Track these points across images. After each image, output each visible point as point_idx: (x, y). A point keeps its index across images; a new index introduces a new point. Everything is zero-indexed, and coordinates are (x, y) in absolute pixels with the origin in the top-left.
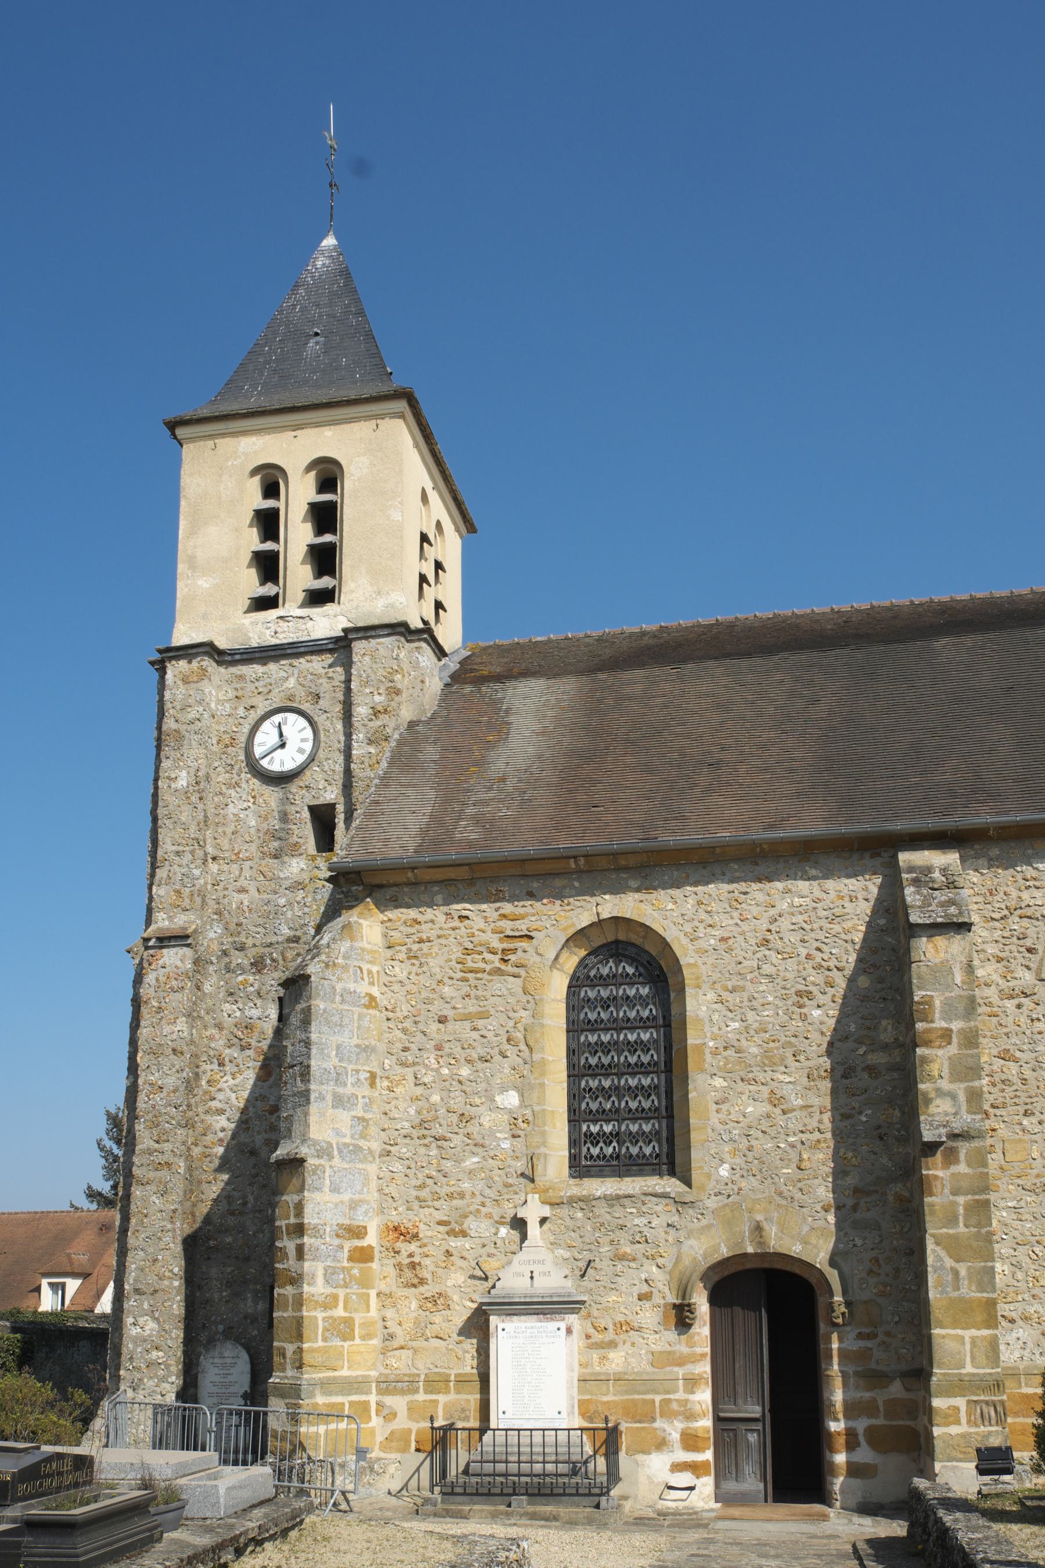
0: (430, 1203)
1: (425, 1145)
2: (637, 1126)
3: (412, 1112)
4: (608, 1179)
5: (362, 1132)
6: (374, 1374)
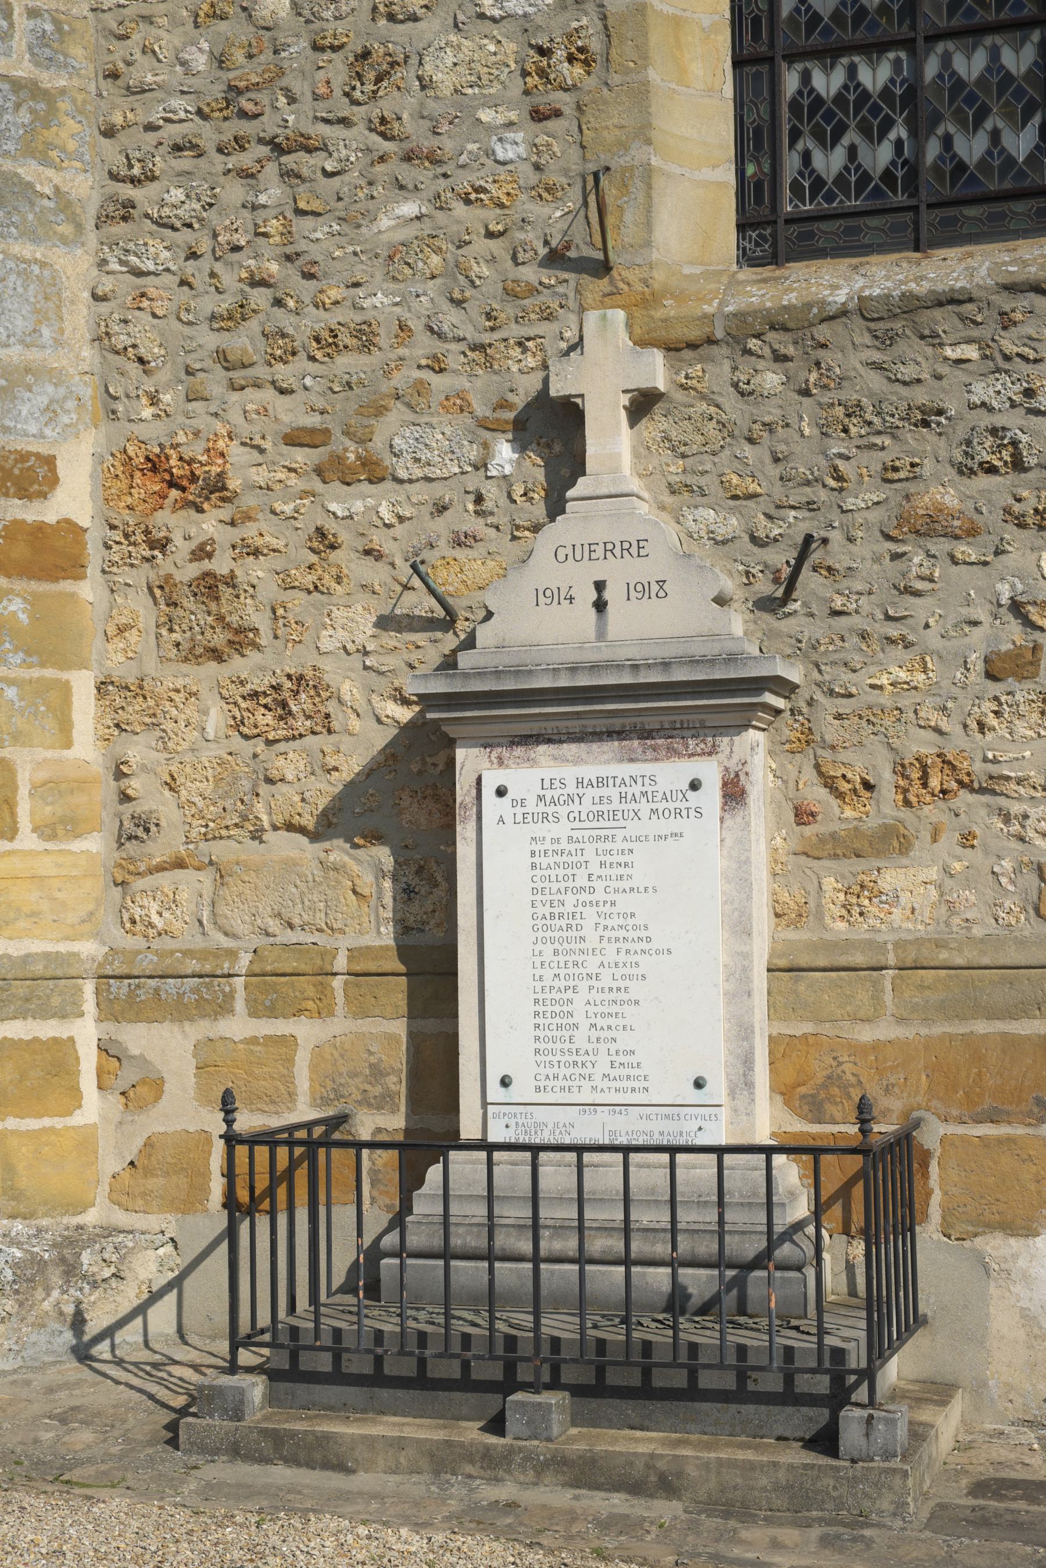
0: (261, 372)
1: (245, 174)
2: (980, 60)
3: (200, 62)
4: (874, 259)
5: (30, 131)
6: (89, 949)
